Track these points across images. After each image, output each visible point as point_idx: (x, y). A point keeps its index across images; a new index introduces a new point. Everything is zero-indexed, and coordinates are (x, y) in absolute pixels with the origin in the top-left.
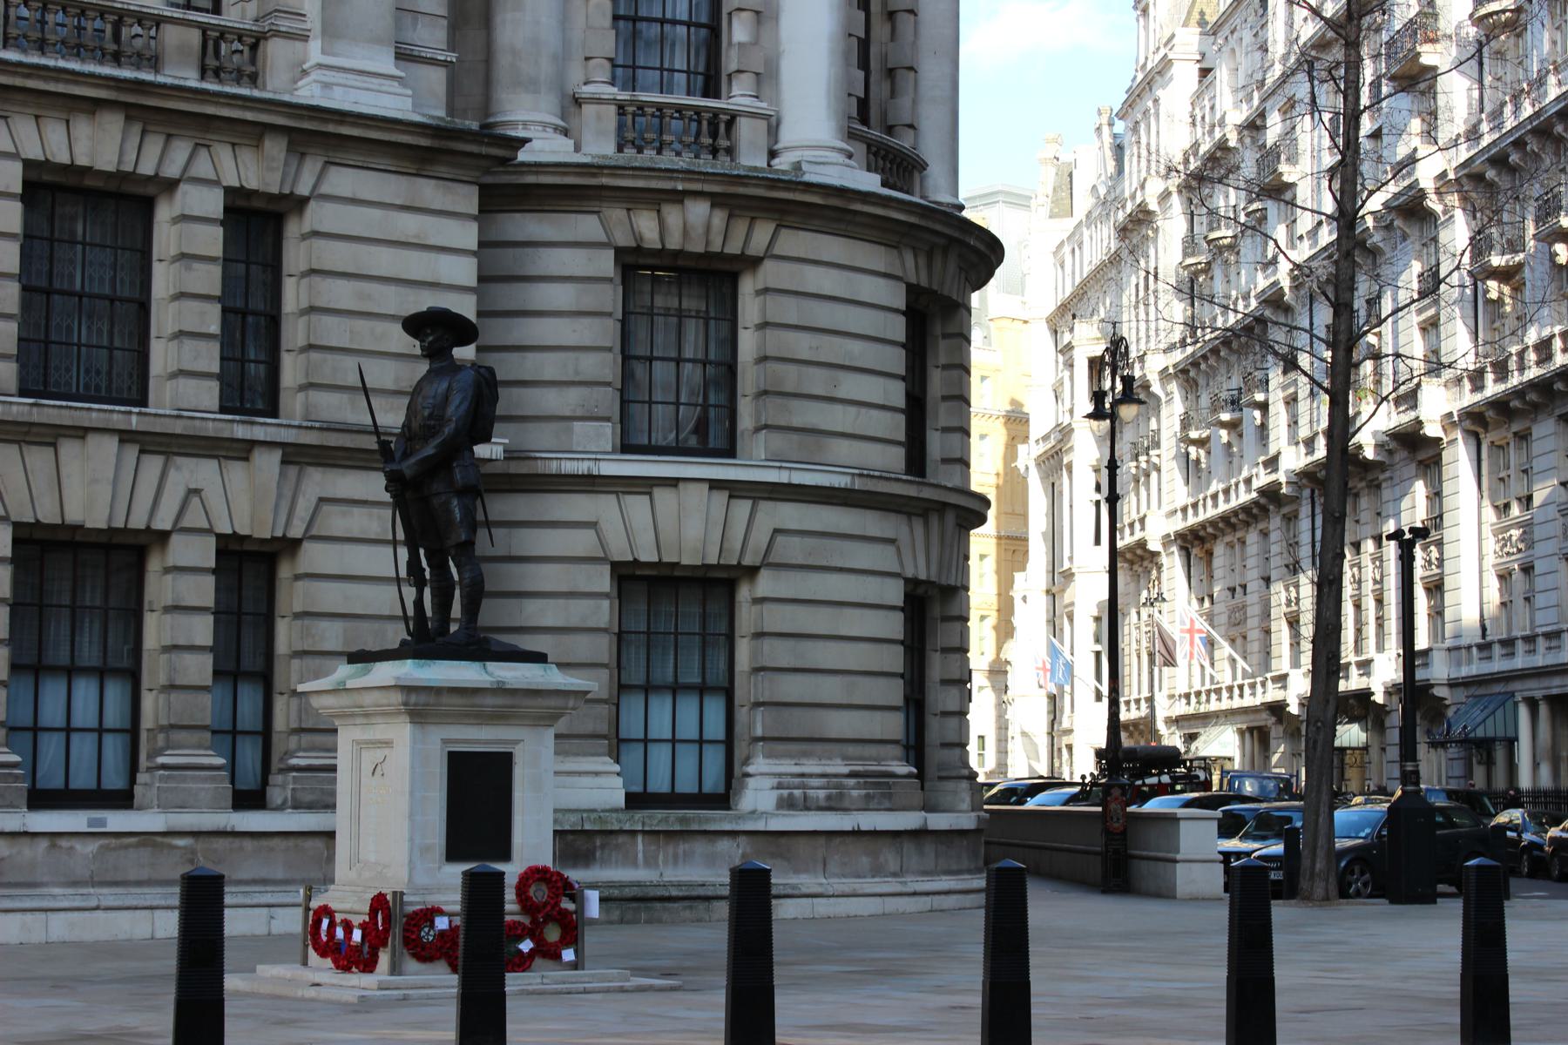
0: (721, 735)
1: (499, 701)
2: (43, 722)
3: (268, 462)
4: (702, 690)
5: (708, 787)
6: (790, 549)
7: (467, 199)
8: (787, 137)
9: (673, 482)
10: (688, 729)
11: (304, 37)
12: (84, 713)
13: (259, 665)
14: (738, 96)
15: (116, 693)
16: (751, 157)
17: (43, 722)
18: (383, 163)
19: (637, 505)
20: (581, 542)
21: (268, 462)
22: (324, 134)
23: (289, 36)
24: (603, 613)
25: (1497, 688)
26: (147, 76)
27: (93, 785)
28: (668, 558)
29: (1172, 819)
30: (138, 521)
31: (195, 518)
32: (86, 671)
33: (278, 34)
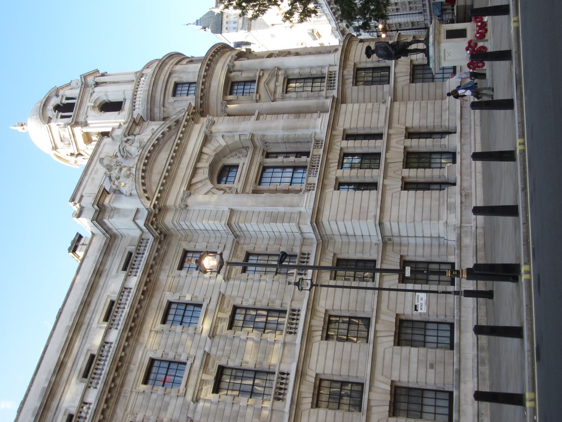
0: (436, 325)
1: (436, 44)
2: (436, 341)
3: (387, 182)
4: (425, 329)
5: (449, 329)
6: (392, 306)
7: (344, 106)
8: (333, 63)
9: (395, 73)
10: (435, 333)
11: (315, 133)
12: (432, 402)
13: (423, 324)
14: (326, 71)
15: (429, 326)
16: (337, 69)
17: (436, 341)
18: (308, 359)
19: (399, 80)
20: (406, 89)
21: (387, 182)
22: (332, 125)
23: (315, 135)
24: (419, 85)
25: (432, 7)
26: (324, 142)
27: (449, 332)
28: (409, 74)
29: (457, 7)
30: (388, 388)
31: (399, 172)
32: (430, 161)
33: (315, 137)
